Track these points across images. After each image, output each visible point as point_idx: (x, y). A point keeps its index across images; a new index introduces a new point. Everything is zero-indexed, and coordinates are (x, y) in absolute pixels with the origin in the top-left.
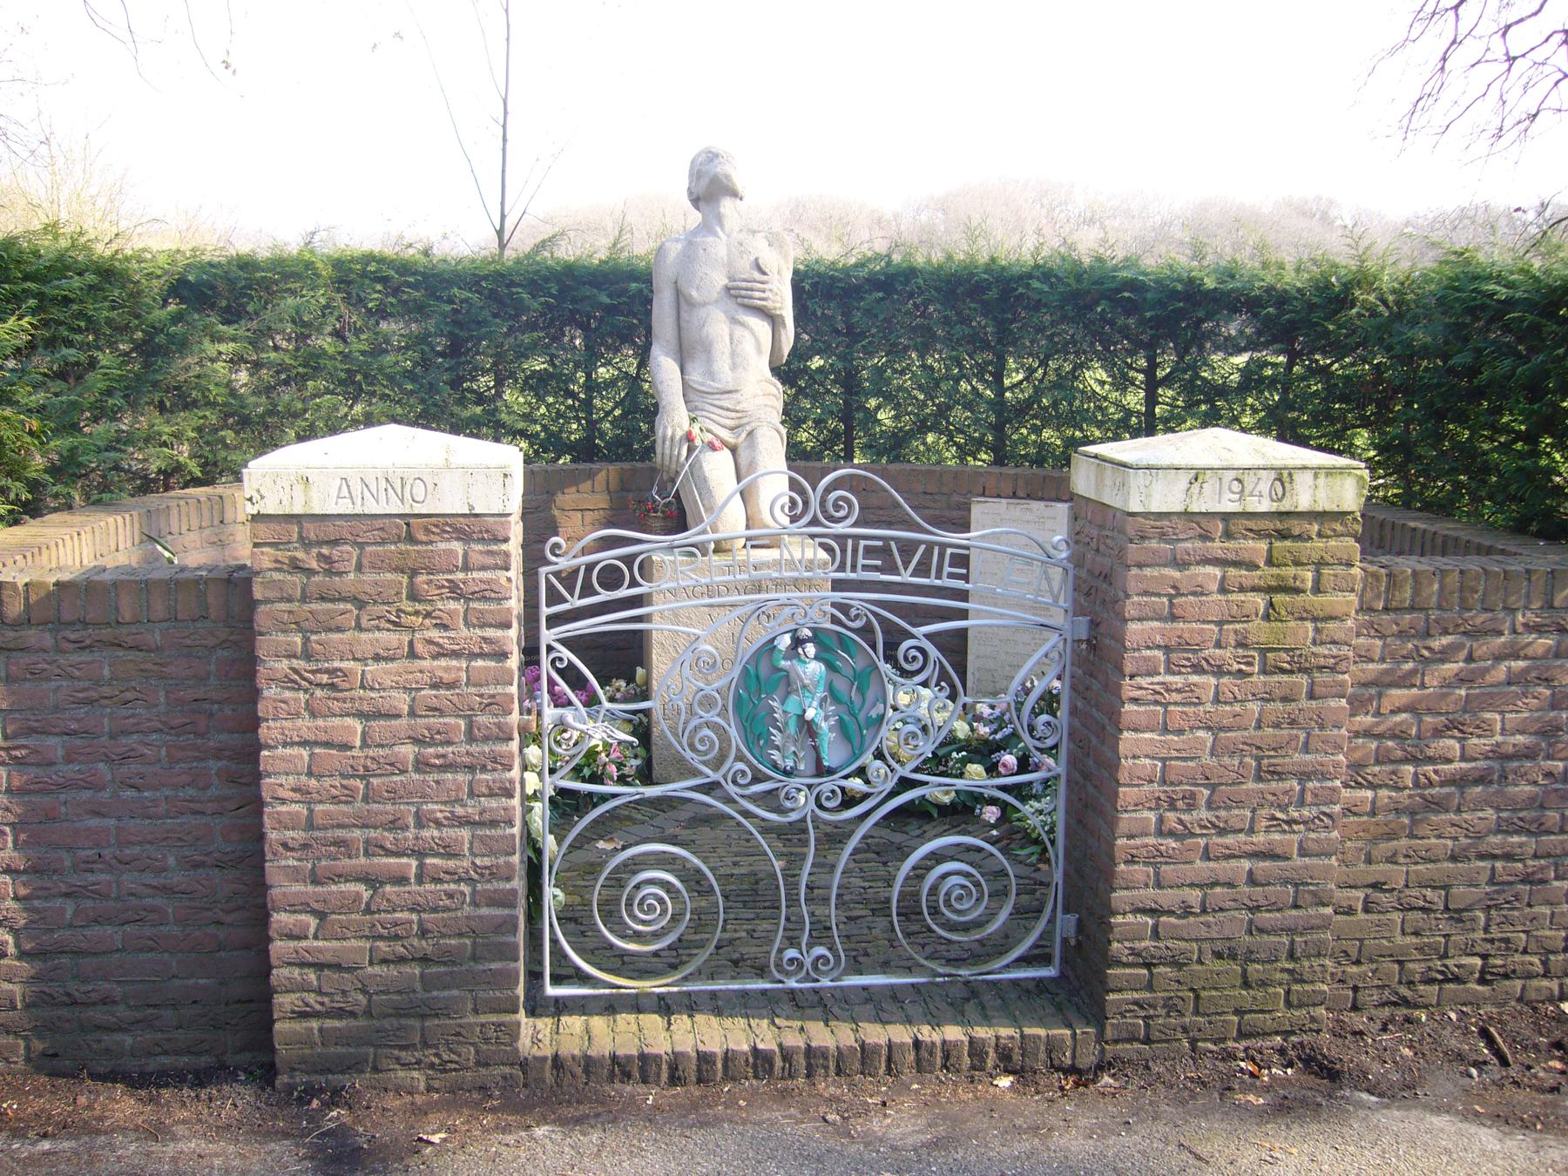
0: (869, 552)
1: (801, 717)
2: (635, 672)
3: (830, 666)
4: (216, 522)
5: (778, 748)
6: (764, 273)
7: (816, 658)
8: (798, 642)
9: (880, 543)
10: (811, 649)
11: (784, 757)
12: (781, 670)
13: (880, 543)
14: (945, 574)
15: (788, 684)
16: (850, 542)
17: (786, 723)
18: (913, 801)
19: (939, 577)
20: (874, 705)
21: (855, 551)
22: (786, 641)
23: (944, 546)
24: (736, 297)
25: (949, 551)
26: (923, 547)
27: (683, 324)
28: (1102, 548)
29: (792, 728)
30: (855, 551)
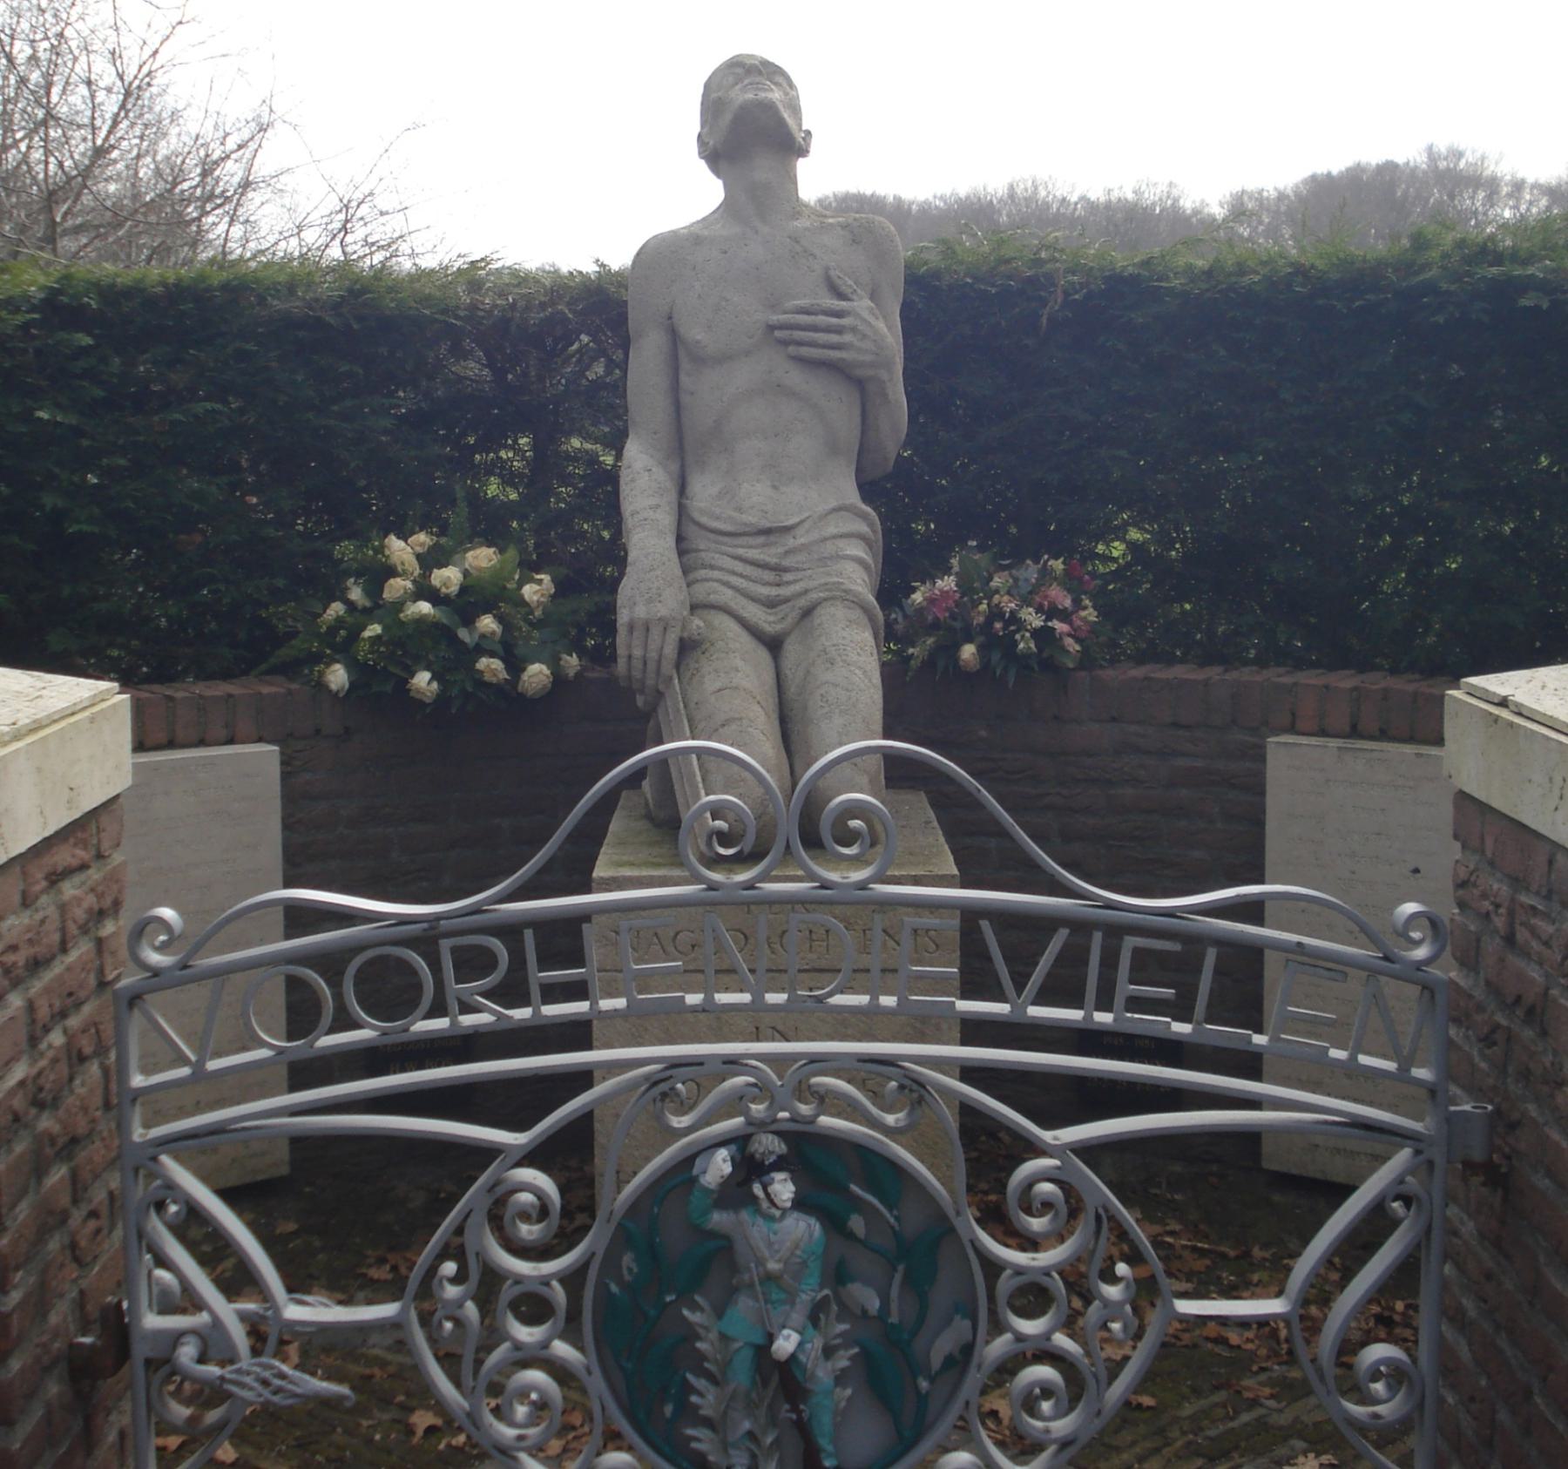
0: (1145, 967)
1: (763, 1350)
2: (698, 1350)
3: (834, 1223)
4: (700, 977)
5: (708, 1423)
6: (842, 296)
7: (799, 1204)
8: (750, 1168)
9: (425, 925)
10: (783, 1188)
11: (725, 1446)
12: (712, 1235)
13: (1175, 947)
14: (1119, 1000)
15: (716, 1265)
16: (1098, 937)
17: (727, 1364)
18: (370, 1302)
19: (1104, 1004)
20: (948, 1322)
21: (1109, 962)
22: (721, 1164)
23: (1115, 932)
24: (785, 343)
25: (1131, 942)
26: (1063, 933)
27: (685, 399)
28: (1522, 935)
29: (741, 1374)
30: (1109, 962)
